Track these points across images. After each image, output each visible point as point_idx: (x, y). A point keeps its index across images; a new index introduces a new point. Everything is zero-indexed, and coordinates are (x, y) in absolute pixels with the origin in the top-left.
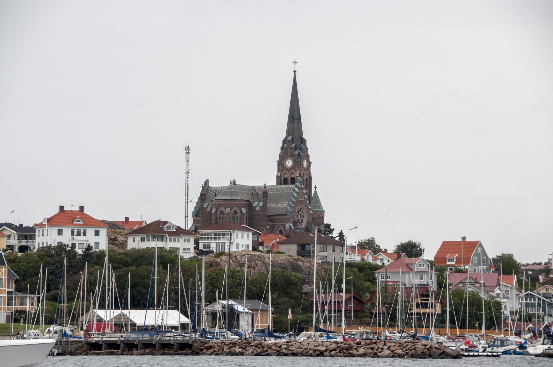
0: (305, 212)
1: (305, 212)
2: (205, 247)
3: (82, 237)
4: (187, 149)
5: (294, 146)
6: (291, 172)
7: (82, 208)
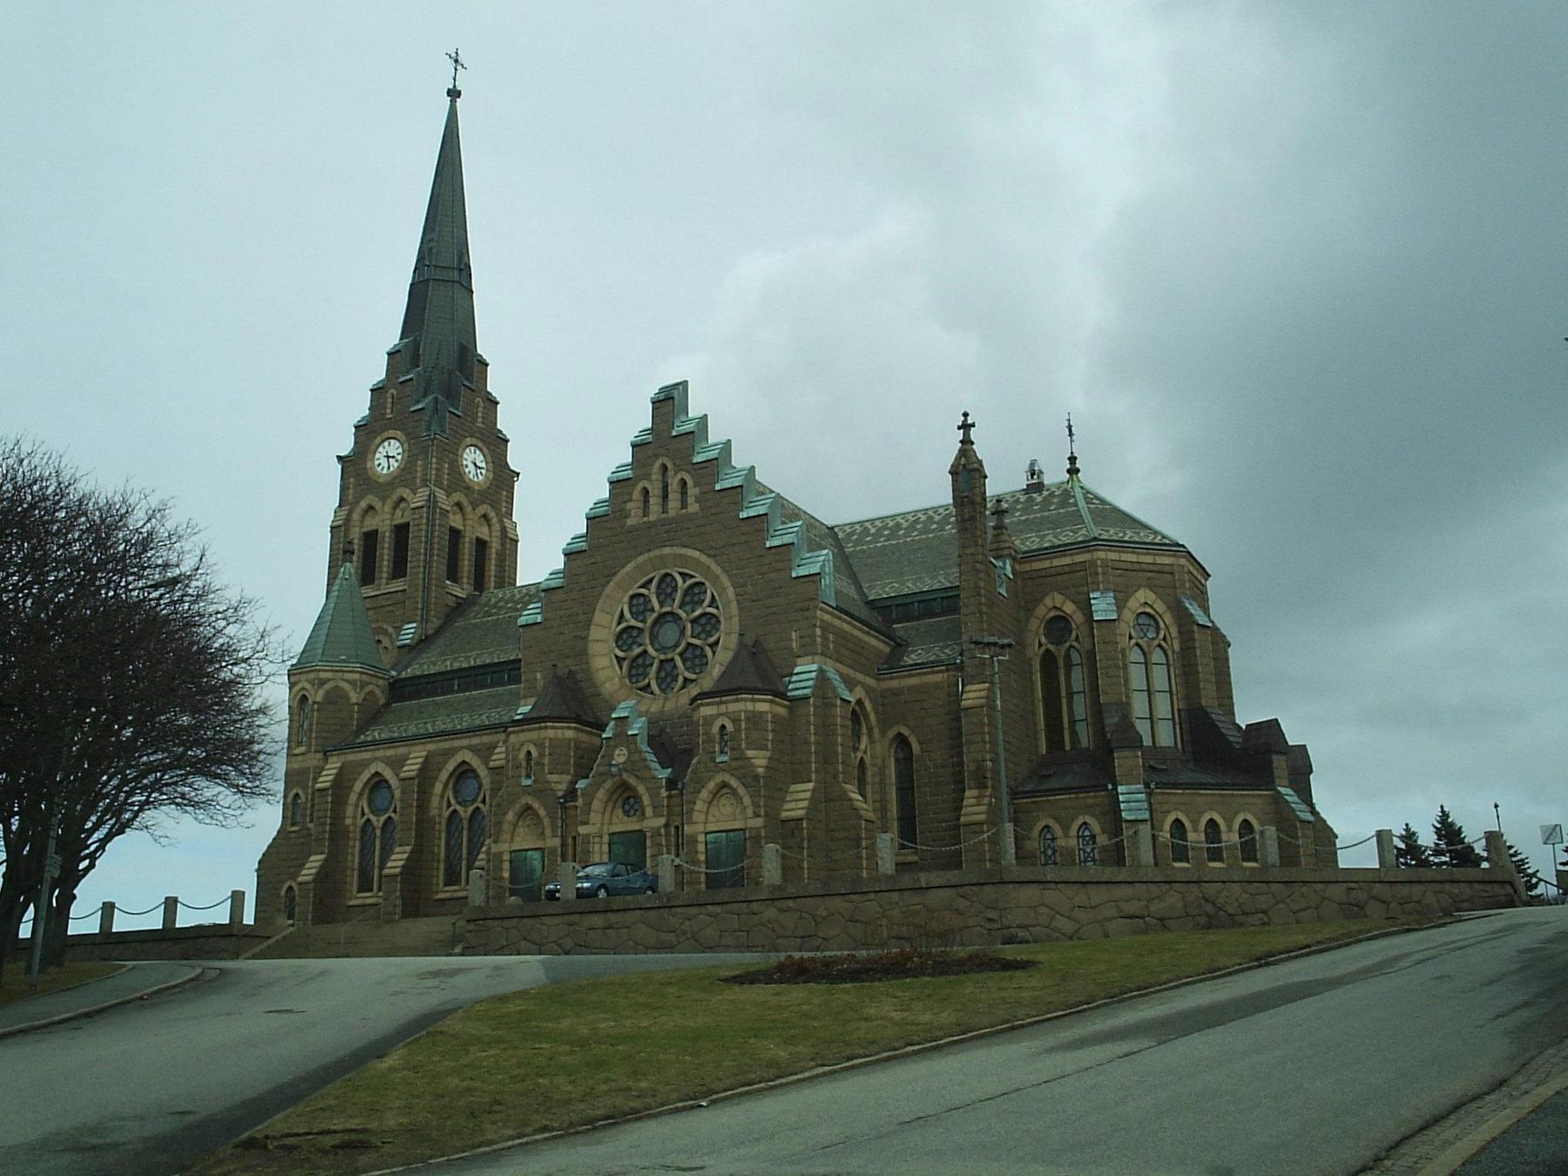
6: (395, 497)
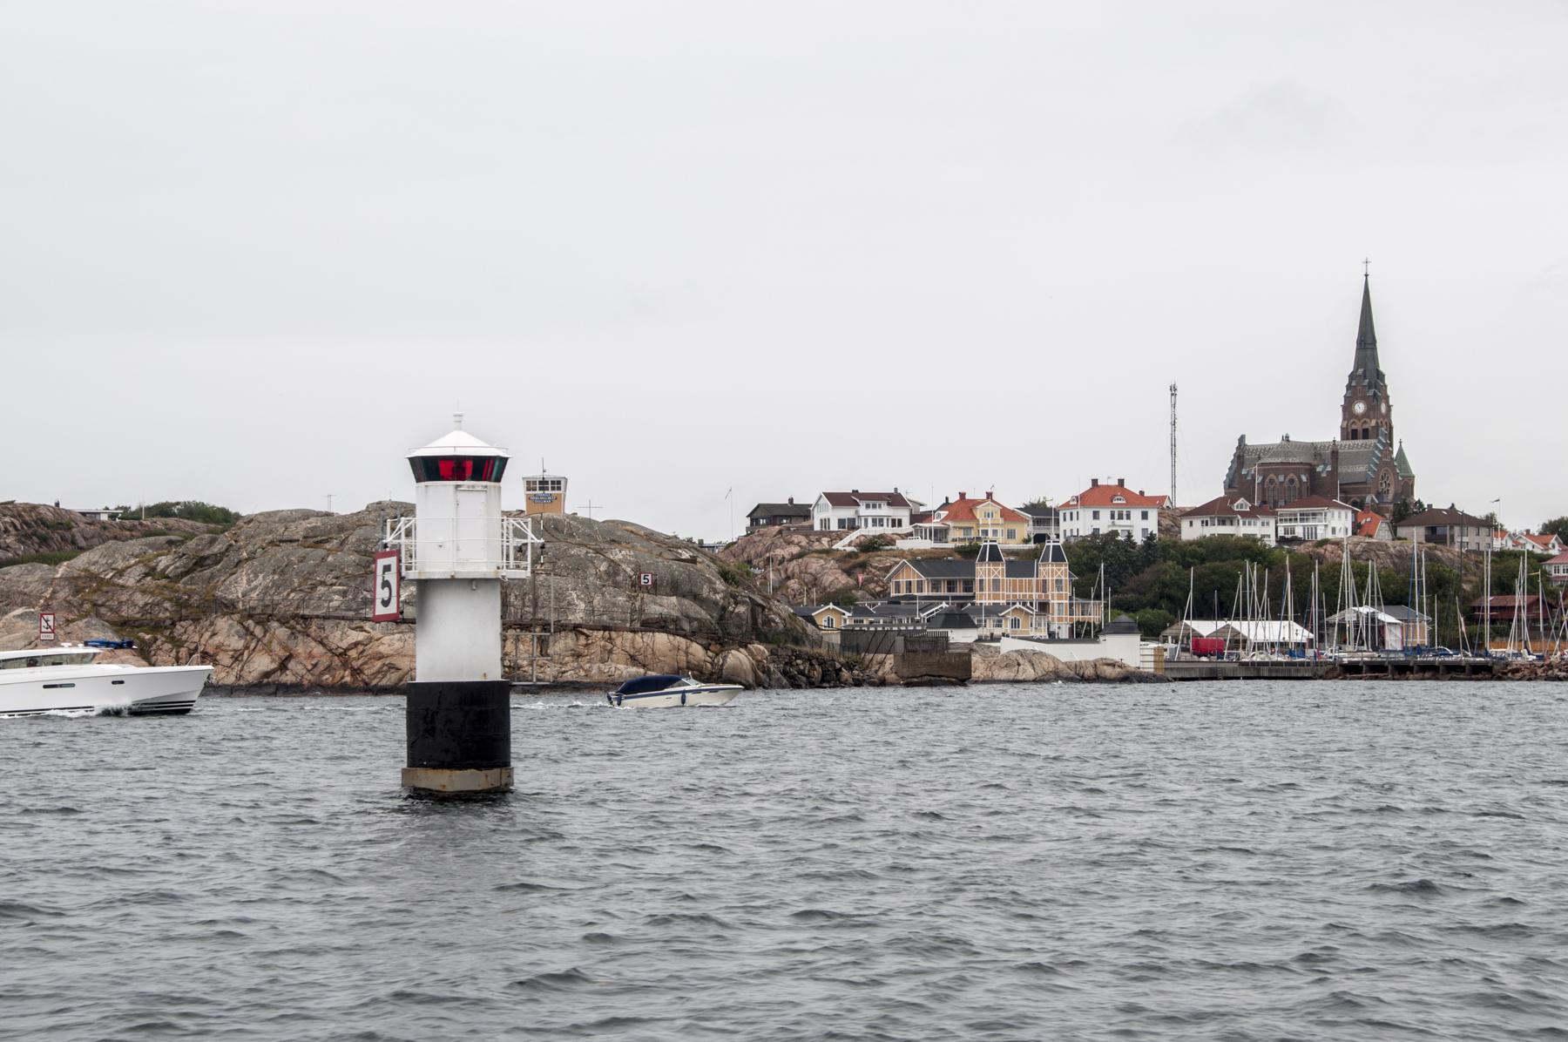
0: (1391, 480)
1: (1391, 480)
2: (1286, 532)
3: (1124, 522)
4: (1173, 389)
5: (1367, 383)
7: (1121, 482)
